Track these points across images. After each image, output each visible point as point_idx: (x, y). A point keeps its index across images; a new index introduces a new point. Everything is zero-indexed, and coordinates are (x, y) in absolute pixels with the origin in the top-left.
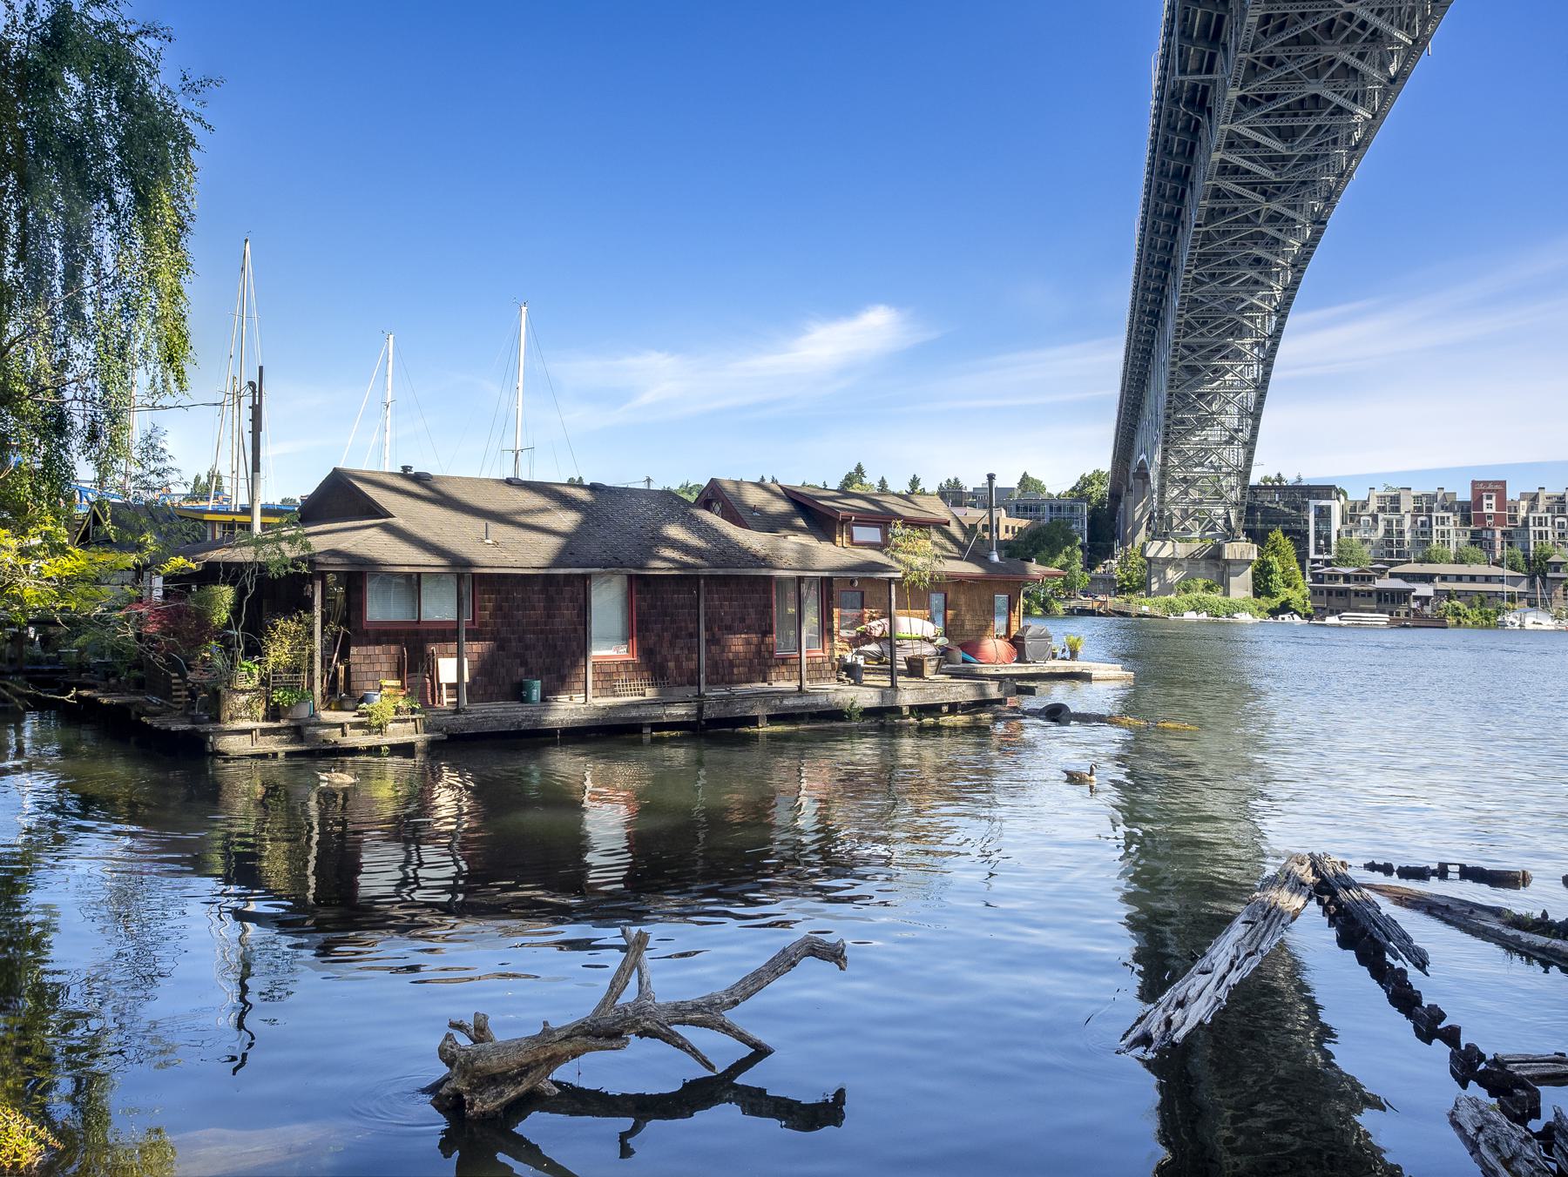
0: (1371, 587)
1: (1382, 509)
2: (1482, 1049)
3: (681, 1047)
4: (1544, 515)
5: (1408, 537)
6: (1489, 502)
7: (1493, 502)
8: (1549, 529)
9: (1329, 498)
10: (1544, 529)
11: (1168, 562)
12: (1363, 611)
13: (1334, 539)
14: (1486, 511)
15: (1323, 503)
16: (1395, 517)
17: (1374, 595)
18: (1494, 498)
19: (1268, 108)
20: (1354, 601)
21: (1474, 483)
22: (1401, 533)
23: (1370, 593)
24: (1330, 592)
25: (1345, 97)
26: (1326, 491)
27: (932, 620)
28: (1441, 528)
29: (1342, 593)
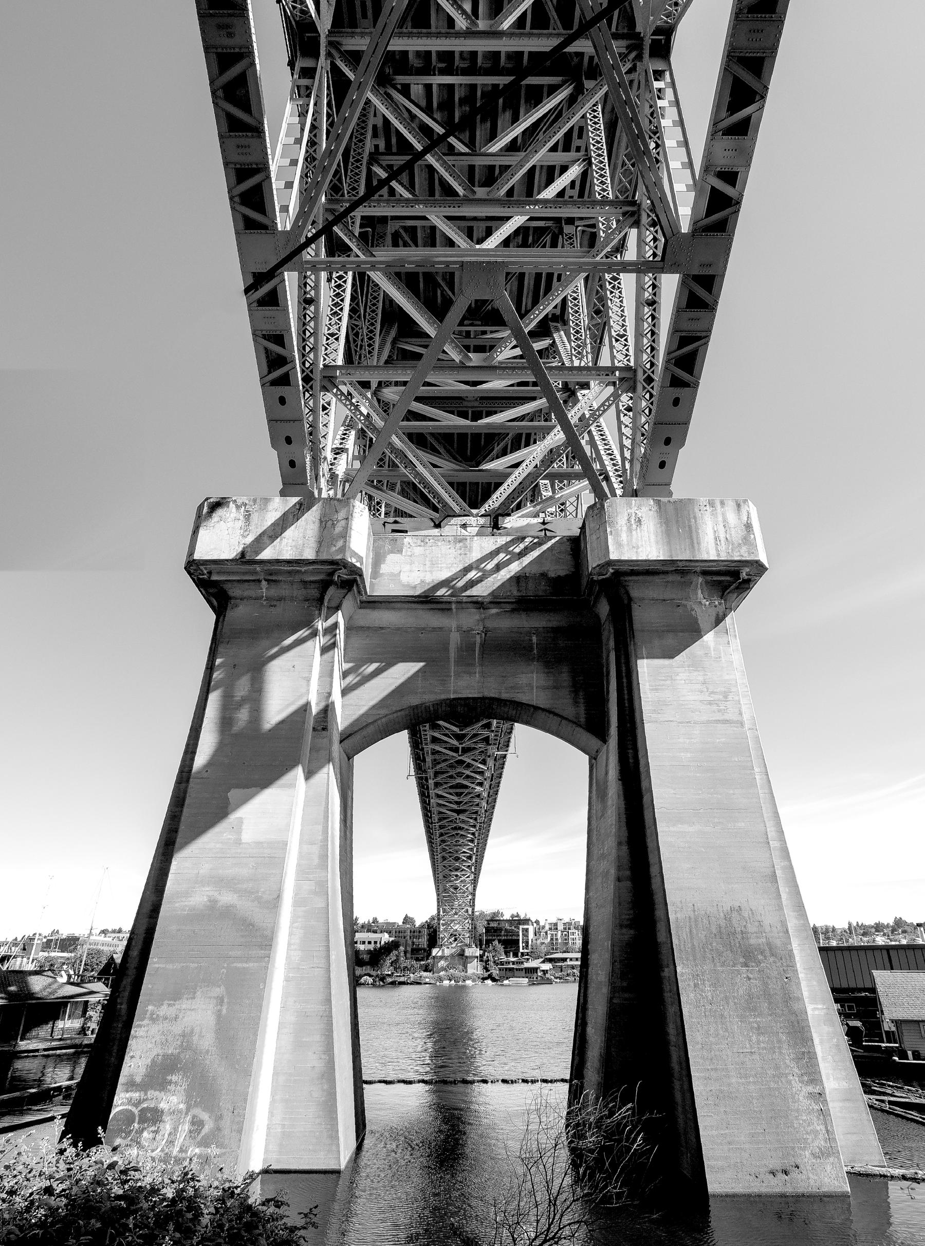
0: (522, 966)
1: (550, 929)
5: (560, 941)
9: (528, 924)
11: (442, 958)
12: (519, 977)
13: (530, 942)
15: (525, 927)
16: (554, 933)
19: (445, 786)
20: (516, 973)
22: (557, 939)
24: (506, 969)
26: (526, 921)
27: (219, 986)
29: (511, 969)
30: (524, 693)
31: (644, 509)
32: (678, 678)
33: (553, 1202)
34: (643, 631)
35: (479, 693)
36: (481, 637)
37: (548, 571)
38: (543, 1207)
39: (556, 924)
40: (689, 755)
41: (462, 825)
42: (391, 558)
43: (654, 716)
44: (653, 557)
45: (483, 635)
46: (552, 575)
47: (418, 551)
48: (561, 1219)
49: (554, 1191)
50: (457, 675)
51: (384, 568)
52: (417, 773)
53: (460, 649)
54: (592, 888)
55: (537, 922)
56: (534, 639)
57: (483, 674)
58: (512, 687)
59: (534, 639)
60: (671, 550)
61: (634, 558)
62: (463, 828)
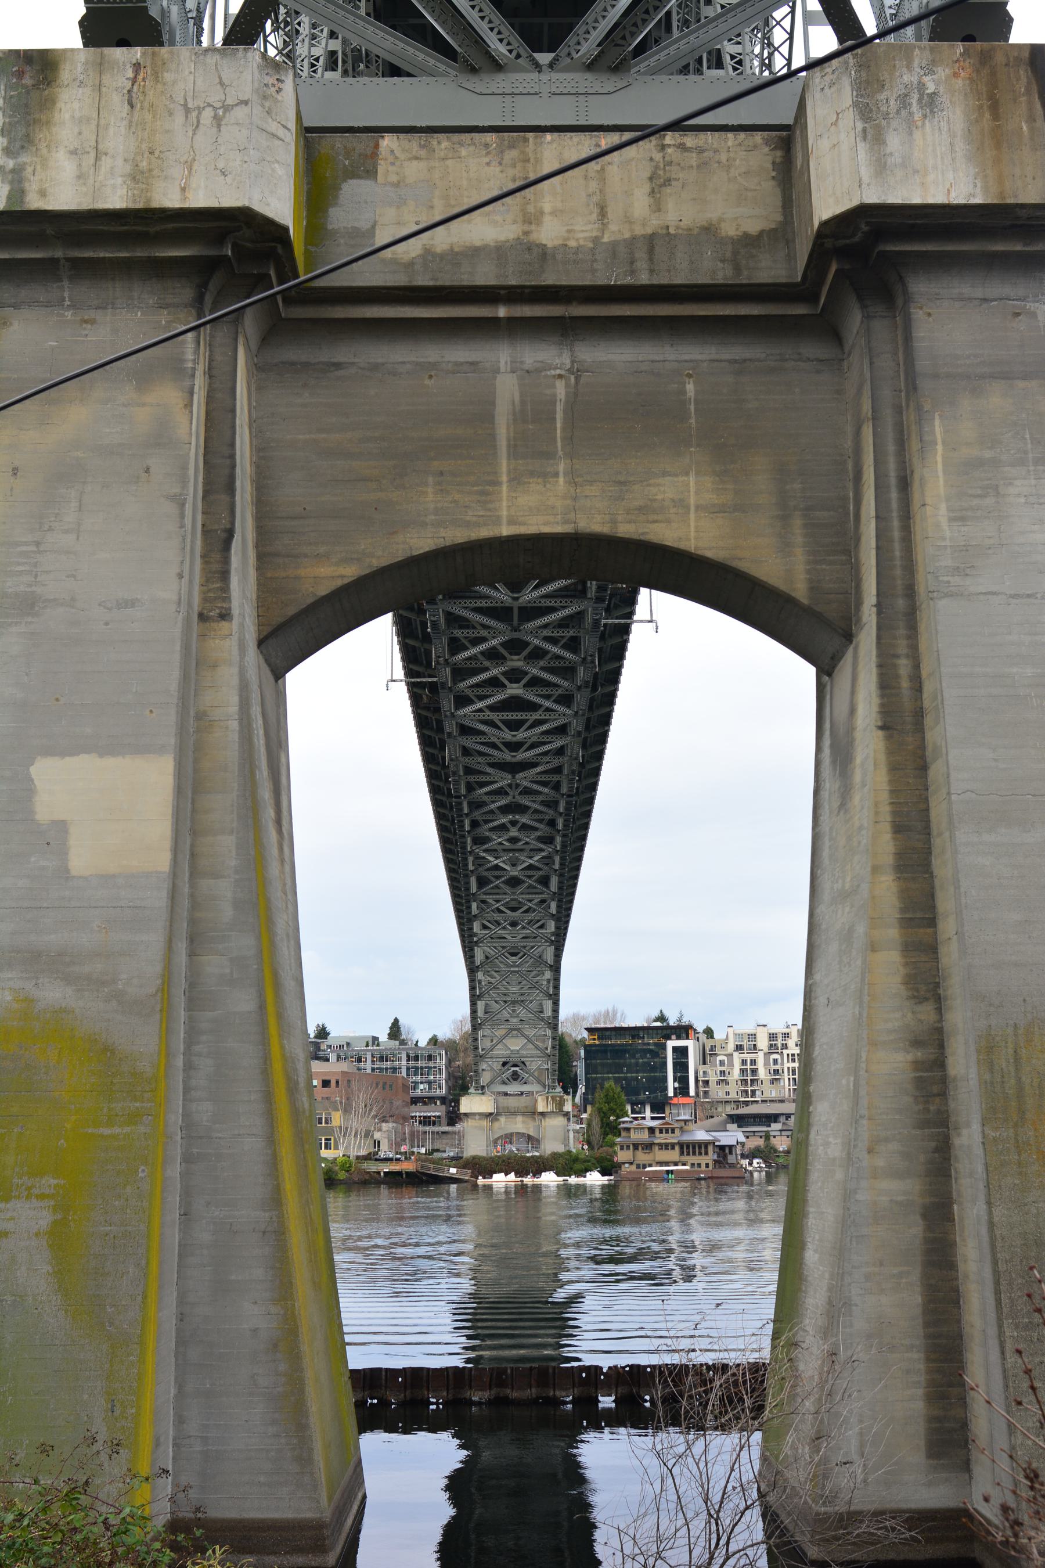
1: (739, 1048)
16: (748, 1057)
17: (677, 1148)
26: (684, 1030)
30: (669, 521)
31: (942, 72)
32: (1012, 490)
33: (714, 1517)
34: (936, 376)
35: (566, 522)
36: (567, 386)
37: (721, 220)
38: (698, 1525)
39: (752, 1036)
40: (1029, 671)
41: (525, 801)
42: (352, 189)
43: (955, 580)
44: (958, 197)
45: (572, 378)
46: (730, 230)
47: (414, 170)
48: (728, 1543)
49: (716, 1498)
50: (516, 480)
51: (339, 217)
52: (409, 673)
53: (519, 417)
54: (820, 965)
55: (709, 1032)
56: (690, 387)
57: (572, 475)
58: (640, 509)
59: (690, 387)
60: (1000, 179)
61: (917, 200)
62: (528, 808)
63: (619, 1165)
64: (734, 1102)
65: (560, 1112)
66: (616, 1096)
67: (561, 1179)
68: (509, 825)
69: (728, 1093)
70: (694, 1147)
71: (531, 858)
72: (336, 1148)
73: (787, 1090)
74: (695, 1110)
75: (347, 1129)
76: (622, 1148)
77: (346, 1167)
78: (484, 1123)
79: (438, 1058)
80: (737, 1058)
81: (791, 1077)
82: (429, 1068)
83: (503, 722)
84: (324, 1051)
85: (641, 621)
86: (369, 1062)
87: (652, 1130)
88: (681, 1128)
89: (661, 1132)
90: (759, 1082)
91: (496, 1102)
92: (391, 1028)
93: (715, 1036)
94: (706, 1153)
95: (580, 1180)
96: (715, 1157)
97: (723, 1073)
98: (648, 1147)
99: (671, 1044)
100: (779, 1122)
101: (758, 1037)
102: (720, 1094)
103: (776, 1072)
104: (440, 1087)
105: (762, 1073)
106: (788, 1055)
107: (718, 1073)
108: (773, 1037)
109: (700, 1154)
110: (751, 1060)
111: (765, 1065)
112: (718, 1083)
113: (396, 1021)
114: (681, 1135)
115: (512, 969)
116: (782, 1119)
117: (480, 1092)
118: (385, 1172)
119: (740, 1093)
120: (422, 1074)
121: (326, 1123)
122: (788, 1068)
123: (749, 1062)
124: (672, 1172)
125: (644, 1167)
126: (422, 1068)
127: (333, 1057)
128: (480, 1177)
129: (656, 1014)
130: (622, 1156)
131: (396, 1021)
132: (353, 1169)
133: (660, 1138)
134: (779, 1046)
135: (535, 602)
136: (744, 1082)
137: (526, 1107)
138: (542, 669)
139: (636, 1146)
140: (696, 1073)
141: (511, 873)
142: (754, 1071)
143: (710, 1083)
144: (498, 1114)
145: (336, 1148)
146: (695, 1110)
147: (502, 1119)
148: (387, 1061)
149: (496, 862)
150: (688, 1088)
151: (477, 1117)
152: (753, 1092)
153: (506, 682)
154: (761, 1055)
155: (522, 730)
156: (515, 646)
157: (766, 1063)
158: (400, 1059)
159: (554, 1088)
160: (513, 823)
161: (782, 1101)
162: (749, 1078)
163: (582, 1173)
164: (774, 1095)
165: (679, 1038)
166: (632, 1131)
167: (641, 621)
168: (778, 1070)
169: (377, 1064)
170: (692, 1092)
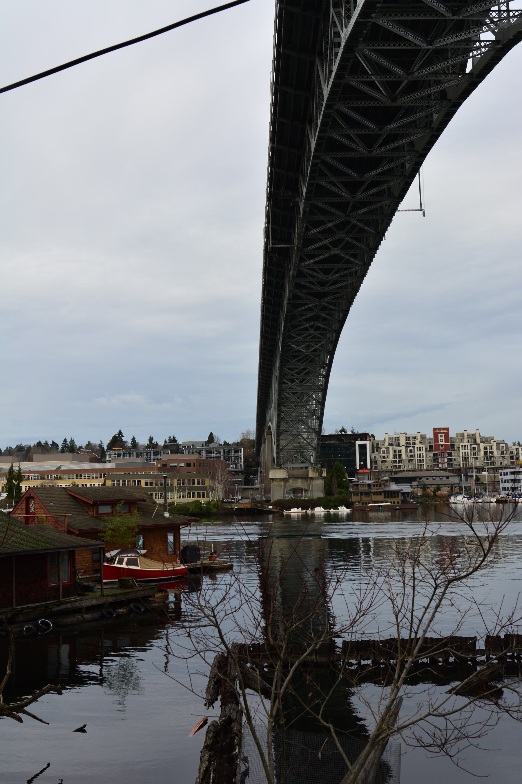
1: (391, 444)
2: (95, 442)
3: (218, 534)
4: (466, 444)
6: (441, 438)
7: (443, 438)
8: (469, 451)
10: (466, 451)
14: (440, 443)
16: (397, 449)
17: (383, 494)
18: (443, 436)
21: (434, 429)
23: (380, 493)
25: (393, 168)
26: (364, 436)
28: (419, 452)
63: (353, 503)
64: (390, 471)
65: (320, 477)
66: (340, 469)
67: (326, 510)
68: (309, 328)
69: (387, 467)
70: (388, 494)
71: (316, 345)
72: (208, 497)
73: (417, 465)
74: (370, 476)
75: (213, 487)
76: (354, 495)
77: (216, 506)
78: (282, 483)
79: (240, 452)
80: (391, 449)
81: (419, 458)
82: (235, 457)
83: (320, 269)
84: (181, 449)
85: (403, 211)
86: (204, 454)
87: (369, 485)
88: (384, 484)
89: (374, 486)
90: (403, 461)
91: (288, 472)
92: (209, 438)
93: (376, 439)
94: (398, 497)
95: (336, 511)
96: (402, 498)
97: (384, 457)
98: (368, 494)
99: (358, 443)
100: (416, 481)
101: (401, 438)
102: (383, 467)
103: (411, 456)
104: (241, 466)
105: (404, 457)
106: (417, 447)
107: (382, 457)
108: (408, 439)
109: (395, 497)
110: (399, 451)
111: (497, 449)
112: (382, 462)
113: (211, 434)
114: (384, 487)
115: (300, 404)
116: (418, 480)
117: (279, 467)
118: (235, 509)
119: (393, 467)
120: (232, 460)
121: (202, 484)
122: (417, 454)
123: (397, 451)
124: (381, 506)
125: (366, 504)
126: (231, 457)
127: (186, 452)
128: (284, 510)
129: (340, 428)
130: (355, 498)
131: (211, 434)
132: (219, 507)
133: (374, 489)
134: (411, 443)
135: (364, 199)
136: (395, 461)
137: (303, 475)
138: (352, 238)
139: (362, 494)
140: (371, 457)
141: (306, 354)
142: (400, 456)
143: (378, 462)
144: (289, 478)
145: (208, 497)
146: (370, 476)
147: (291, 481)
148: (213, 454)
149: (298, 348)
150: (367, 465)
151: (278, 480)
152: (400, 466)
153: (331, 247)
154: (403, 448)
155: (331, 274)
156: (341, 226)
157: (406, 452)
158: (220, 452)
159: (317, 465)
160: (311, 327)
161: (414, 471)
162: (397, 460)
163: (336, 508)
164: (410, 467)
165: (361, 440)
166: (359, 486)
167: (403, 211)
168: (412, 455)
169: (209, 455)
170: (369, 467)
